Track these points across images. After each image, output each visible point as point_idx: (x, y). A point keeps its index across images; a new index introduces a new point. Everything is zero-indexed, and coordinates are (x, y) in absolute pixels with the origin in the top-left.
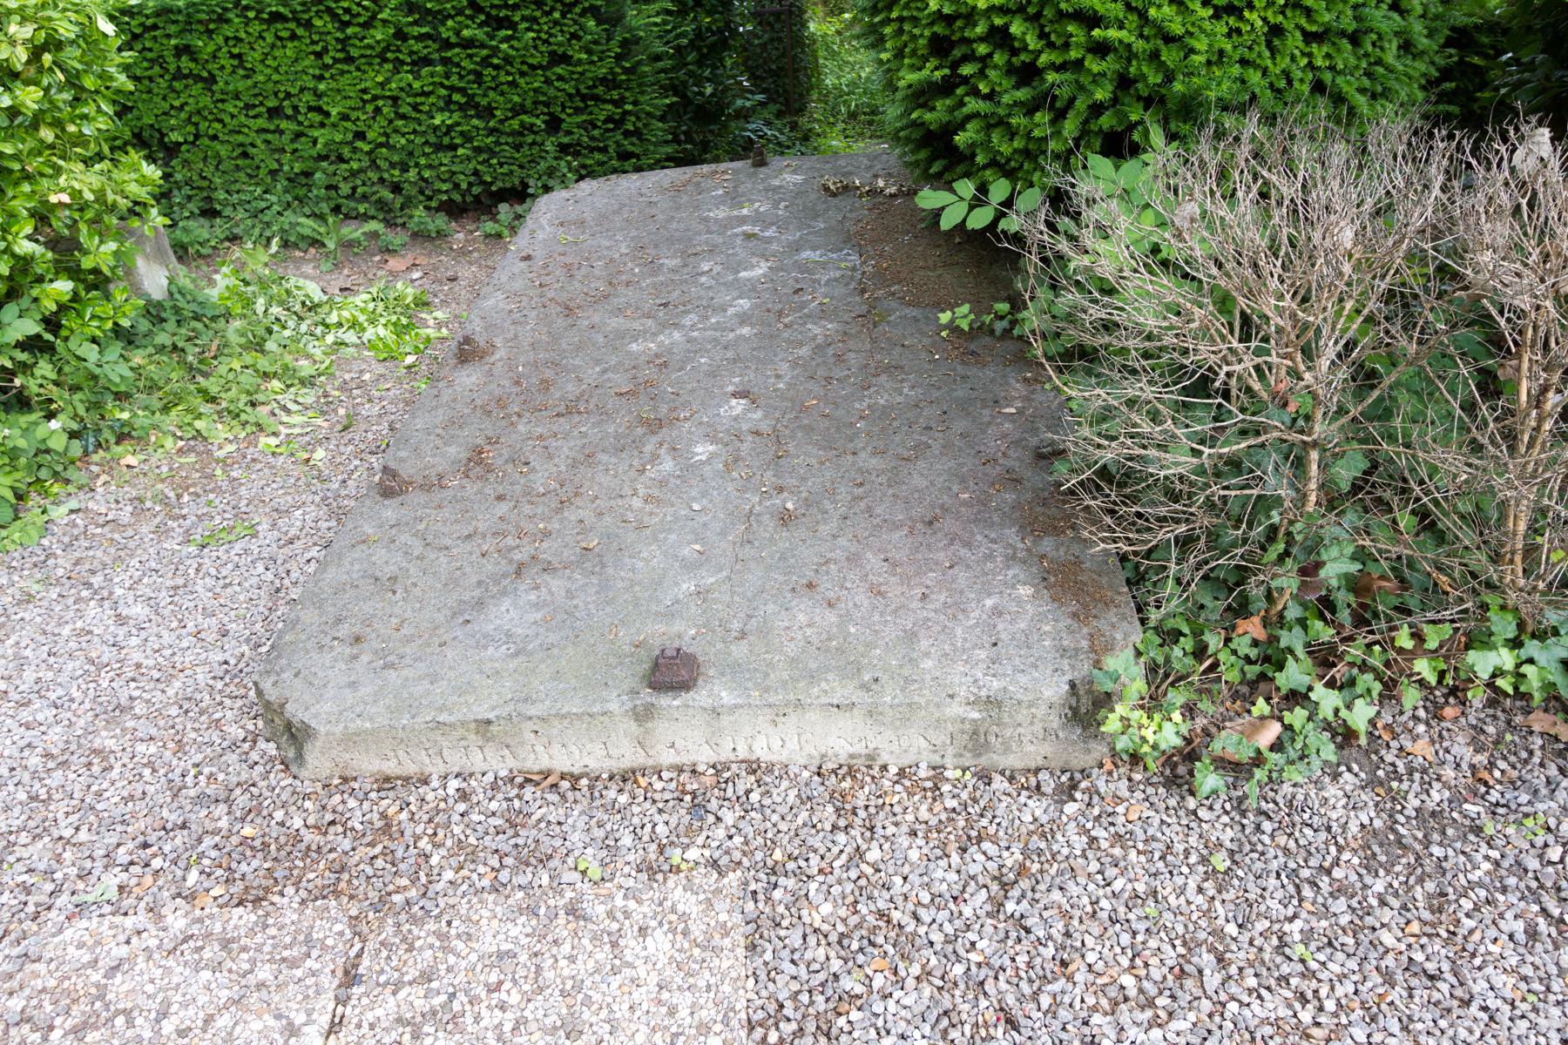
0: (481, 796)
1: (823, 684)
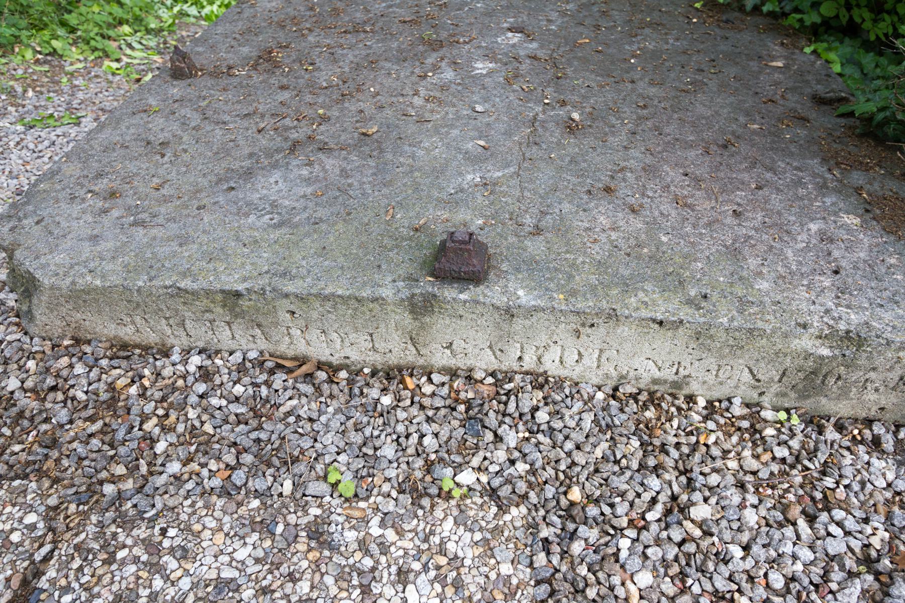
0: (225, 378)
1: (641, 294)
